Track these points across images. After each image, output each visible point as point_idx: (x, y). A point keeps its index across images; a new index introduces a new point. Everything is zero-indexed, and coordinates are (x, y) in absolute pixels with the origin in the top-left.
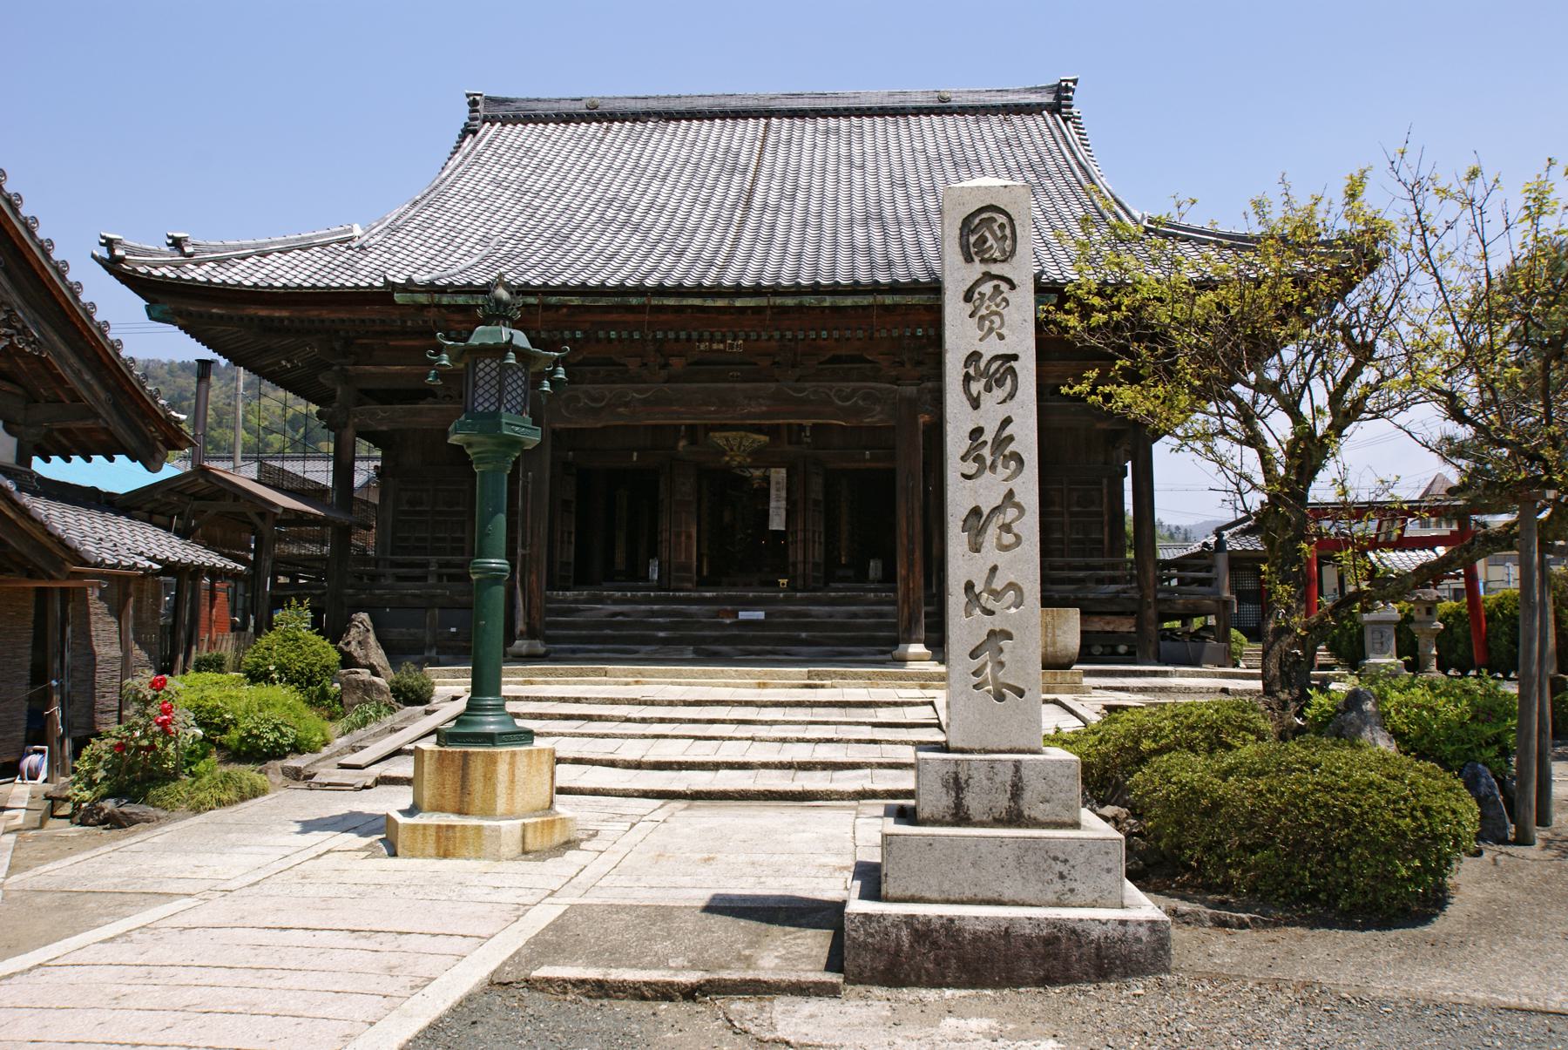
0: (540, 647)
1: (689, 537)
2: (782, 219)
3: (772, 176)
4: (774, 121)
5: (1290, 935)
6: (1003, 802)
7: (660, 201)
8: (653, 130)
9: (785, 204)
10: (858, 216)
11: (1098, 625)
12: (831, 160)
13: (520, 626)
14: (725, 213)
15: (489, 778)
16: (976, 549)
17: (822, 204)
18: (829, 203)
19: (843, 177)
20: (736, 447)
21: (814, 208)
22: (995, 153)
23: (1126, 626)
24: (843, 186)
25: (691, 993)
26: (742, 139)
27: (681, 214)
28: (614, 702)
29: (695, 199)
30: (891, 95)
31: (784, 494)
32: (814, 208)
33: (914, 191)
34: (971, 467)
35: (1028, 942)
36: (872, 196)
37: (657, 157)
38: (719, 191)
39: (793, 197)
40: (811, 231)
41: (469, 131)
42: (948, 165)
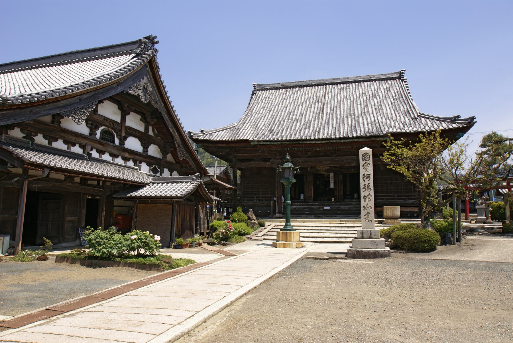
0: (281, 215)
1: (311, 190)
2: (331, 116)
3: (328, 103)
4: (327, 86)
5: (409, 254)
6: (369, 236)
7: (302, 112)
8: (298, 91)
9: (332, 112)
10: (349, 115)
11: (404, 209)
12: (342, 97)
13: (277, 211)
14: (318, 115)
15: (290, 236)
16: (365, 201)
17: (340, 111)
18: (342, 111)
19: (345, 103)
20: (322, 169)
21: (338, 113)
22: (383, 93)
23: (416, 209)
24: (345, 105)
25: (327, 259)
26: (320, 92)
27: (307, 116)
28: (300, 226)
29: (310, 111)
30: (357, 77)
31: (333, 179)
32: (338, 113)
33: (362, 106)
34: (364, 190)
35: (372, 253)
36: (352, 108)
37: (300, 99)
38: (316, 108)
39: (333, 109)
40: (338, 120)
41: (254, 93)
42: (371, 97)
